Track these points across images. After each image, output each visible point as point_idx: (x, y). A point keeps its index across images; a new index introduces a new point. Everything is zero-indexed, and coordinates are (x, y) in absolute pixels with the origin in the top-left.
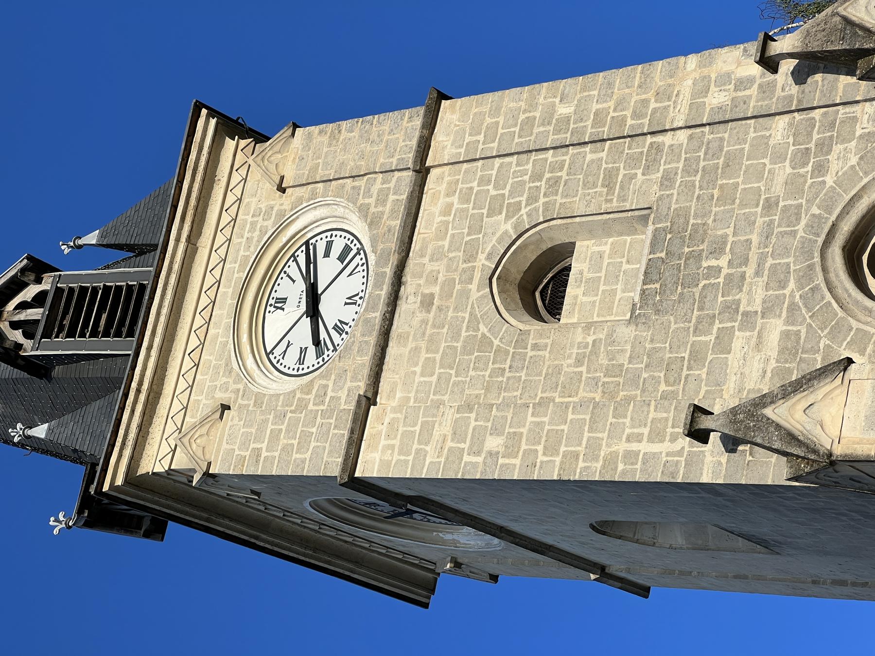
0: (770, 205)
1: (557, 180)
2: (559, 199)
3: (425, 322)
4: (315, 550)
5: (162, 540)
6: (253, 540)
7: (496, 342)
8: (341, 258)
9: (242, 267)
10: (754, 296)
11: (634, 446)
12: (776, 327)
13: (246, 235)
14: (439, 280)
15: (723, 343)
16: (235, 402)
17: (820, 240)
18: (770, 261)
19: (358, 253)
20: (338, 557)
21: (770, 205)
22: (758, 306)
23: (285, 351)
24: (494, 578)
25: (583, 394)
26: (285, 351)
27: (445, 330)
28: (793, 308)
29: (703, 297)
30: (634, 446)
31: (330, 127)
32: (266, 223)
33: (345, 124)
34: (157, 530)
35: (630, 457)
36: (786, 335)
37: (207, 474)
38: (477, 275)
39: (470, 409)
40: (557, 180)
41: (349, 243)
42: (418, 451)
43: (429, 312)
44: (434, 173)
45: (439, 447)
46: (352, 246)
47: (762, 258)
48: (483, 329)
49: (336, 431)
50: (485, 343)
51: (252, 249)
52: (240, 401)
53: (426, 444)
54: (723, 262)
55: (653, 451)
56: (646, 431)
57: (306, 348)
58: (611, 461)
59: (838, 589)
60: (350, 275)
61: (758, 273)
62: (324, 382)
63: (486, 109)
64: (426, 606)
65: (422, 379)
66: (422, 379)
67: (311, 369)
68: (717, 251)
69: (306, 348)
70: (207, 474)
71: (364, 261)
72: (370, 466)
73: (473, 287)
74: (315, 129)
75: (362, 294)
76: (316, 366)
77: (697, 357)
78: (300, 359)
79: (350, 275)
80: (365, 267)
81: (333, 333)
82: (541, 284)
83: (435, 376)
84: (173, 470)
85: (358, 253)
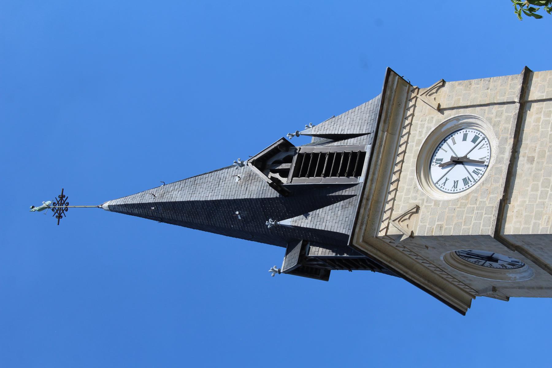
4: (429, 281)
6: (405, 274)
8: (474, 141)
9: (417, 144)
13: (418, 130)
14: (536, 151)
16: (422, 204)
19: (484, 139)
20: (436, 285)
23: (445, 183)
26: (445, 183)
27: (542, 172)
31: (466, 82)
32: (429, 125)
33: (474, 81)
34: (508, 299)
37: (412, 236)
41: (477, 135)
42: (535, 224)
43: (532, 164)
44: (535, 106)
45: (546, 221)
46: (479, 136)
49: (486, 216)
51: (423, 136)
52: (425, 204)
53: (539, 219)
57: (457, 181)
60: (480, 148)
62: (476, 195)
64: (464, 314)
65: (532, 193)
66: (532, 193)
67: (446, 191)
69: (457, 181)
70: (412, 236)
71: (487, 142)
72: (511, 228)
74: (456, 83)
75: (487, 157)
76: (465, 189)
78: (454, 186)
79: (480, 148)
80: (488, 145)
81: (473, 174)
83: (539, 192)
84: (388, 236)
85: (484, 139)
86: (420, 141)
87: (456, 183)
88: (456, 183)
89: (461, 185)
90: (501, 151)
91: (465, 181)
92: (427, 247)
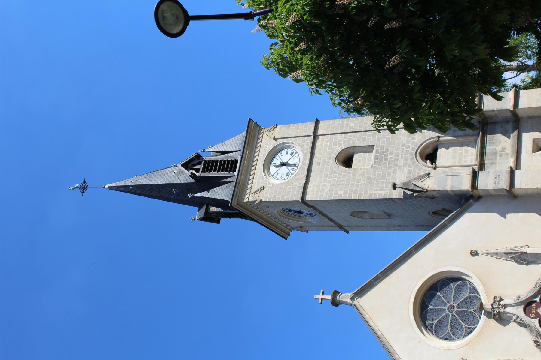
0: (403, 146)
1: (351, 139)
2: (351, 143)
3: (403, 149)
5: (533, 140)
7: (338, 172)
8: (291, 154)
9: (264, 156)
10: (401, 162)
11: (376, 192)
12: (406, 169)
15: (395, 171)
17: (415, 152)
18: (404, 156)
21: (403, 146)
22: (402, 164)
24: (474, 254)
25: (362, 182)
28: (410, 165)
29: (389, 163)
30: (376, 192)
33: (291, 125)
34: (308, 231)
35: (375, 194)
36: (408, 170)
37: (261, 201)
38: (332, 159)
39: (333, 185)
40: (351, 139)
47: (402, 155)
48: (334, 169)
50: (335, 172)
54: (393, 156)
55: (385, 192)
56: (378, 189)
58: (371, 195)
59: (399, 228)
61: (402, 158)
63: (330, 123)
64: (286, 239)
68: (392, 153)
70: (261, 201)
72: (309, 197)
73: (331, 161)
77: (389, 174)
82: (347, 161)
86: (265, 154)
87: (282, 175)
88: (282, 175)
89: (285, 176)
90: (305, 159)
91: (287, 174)
92: (268, 207)
